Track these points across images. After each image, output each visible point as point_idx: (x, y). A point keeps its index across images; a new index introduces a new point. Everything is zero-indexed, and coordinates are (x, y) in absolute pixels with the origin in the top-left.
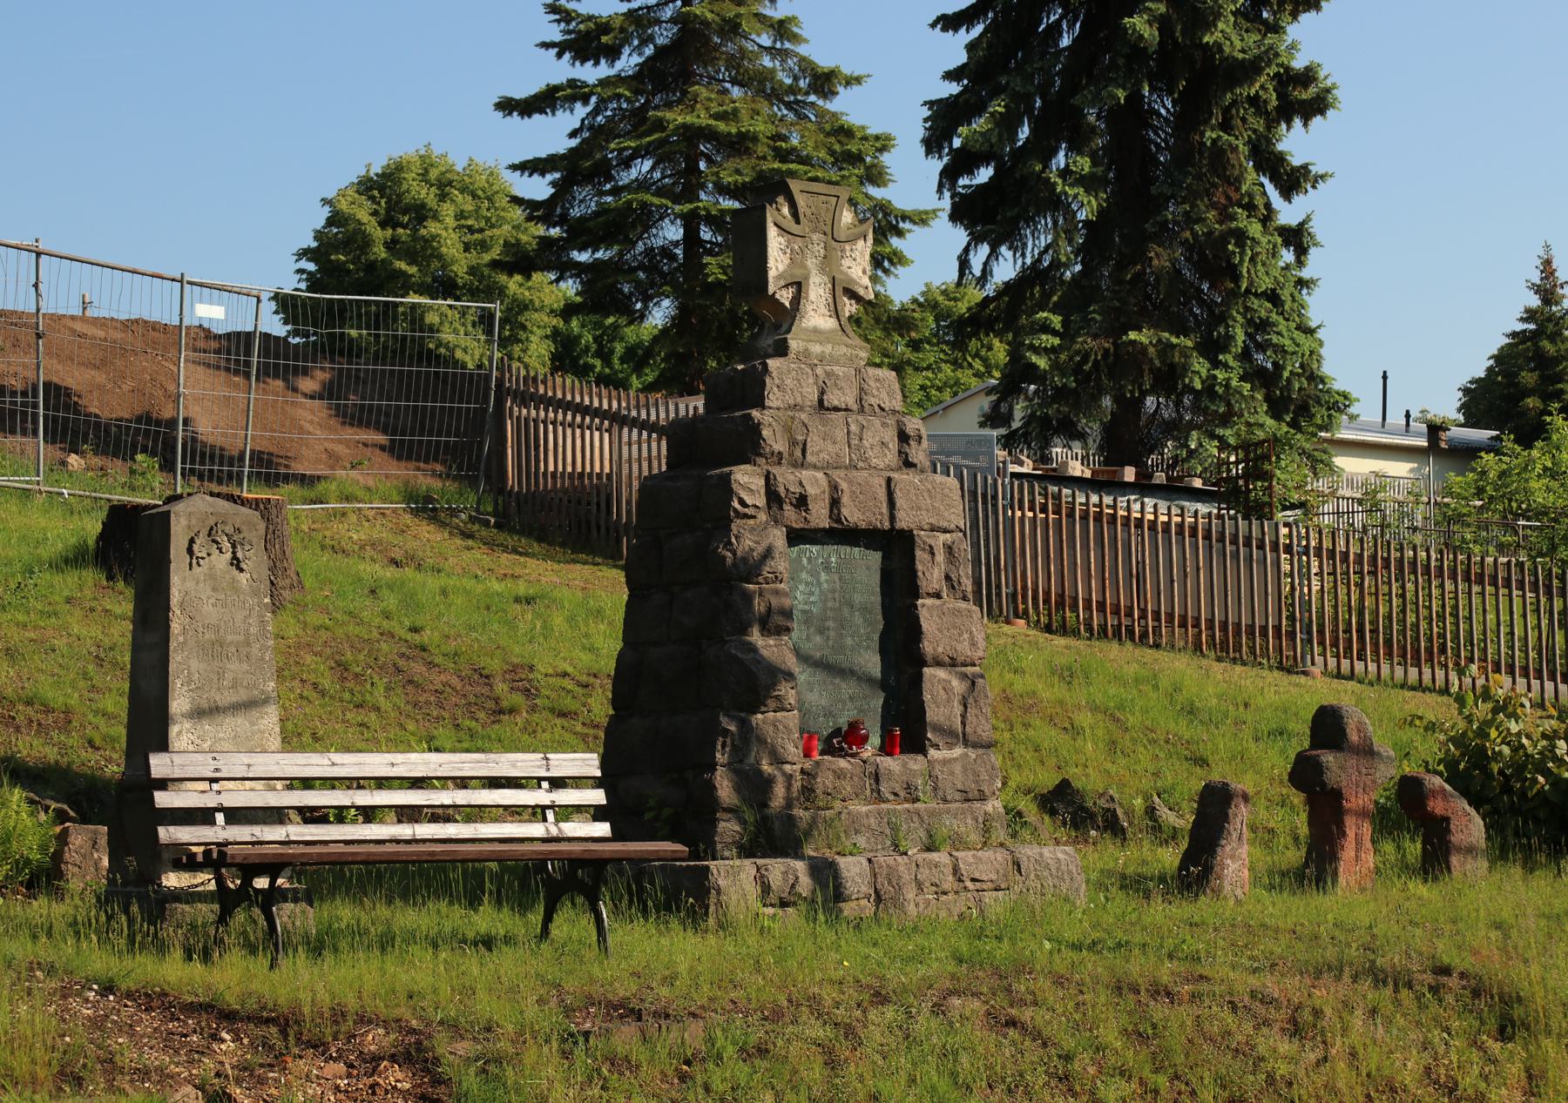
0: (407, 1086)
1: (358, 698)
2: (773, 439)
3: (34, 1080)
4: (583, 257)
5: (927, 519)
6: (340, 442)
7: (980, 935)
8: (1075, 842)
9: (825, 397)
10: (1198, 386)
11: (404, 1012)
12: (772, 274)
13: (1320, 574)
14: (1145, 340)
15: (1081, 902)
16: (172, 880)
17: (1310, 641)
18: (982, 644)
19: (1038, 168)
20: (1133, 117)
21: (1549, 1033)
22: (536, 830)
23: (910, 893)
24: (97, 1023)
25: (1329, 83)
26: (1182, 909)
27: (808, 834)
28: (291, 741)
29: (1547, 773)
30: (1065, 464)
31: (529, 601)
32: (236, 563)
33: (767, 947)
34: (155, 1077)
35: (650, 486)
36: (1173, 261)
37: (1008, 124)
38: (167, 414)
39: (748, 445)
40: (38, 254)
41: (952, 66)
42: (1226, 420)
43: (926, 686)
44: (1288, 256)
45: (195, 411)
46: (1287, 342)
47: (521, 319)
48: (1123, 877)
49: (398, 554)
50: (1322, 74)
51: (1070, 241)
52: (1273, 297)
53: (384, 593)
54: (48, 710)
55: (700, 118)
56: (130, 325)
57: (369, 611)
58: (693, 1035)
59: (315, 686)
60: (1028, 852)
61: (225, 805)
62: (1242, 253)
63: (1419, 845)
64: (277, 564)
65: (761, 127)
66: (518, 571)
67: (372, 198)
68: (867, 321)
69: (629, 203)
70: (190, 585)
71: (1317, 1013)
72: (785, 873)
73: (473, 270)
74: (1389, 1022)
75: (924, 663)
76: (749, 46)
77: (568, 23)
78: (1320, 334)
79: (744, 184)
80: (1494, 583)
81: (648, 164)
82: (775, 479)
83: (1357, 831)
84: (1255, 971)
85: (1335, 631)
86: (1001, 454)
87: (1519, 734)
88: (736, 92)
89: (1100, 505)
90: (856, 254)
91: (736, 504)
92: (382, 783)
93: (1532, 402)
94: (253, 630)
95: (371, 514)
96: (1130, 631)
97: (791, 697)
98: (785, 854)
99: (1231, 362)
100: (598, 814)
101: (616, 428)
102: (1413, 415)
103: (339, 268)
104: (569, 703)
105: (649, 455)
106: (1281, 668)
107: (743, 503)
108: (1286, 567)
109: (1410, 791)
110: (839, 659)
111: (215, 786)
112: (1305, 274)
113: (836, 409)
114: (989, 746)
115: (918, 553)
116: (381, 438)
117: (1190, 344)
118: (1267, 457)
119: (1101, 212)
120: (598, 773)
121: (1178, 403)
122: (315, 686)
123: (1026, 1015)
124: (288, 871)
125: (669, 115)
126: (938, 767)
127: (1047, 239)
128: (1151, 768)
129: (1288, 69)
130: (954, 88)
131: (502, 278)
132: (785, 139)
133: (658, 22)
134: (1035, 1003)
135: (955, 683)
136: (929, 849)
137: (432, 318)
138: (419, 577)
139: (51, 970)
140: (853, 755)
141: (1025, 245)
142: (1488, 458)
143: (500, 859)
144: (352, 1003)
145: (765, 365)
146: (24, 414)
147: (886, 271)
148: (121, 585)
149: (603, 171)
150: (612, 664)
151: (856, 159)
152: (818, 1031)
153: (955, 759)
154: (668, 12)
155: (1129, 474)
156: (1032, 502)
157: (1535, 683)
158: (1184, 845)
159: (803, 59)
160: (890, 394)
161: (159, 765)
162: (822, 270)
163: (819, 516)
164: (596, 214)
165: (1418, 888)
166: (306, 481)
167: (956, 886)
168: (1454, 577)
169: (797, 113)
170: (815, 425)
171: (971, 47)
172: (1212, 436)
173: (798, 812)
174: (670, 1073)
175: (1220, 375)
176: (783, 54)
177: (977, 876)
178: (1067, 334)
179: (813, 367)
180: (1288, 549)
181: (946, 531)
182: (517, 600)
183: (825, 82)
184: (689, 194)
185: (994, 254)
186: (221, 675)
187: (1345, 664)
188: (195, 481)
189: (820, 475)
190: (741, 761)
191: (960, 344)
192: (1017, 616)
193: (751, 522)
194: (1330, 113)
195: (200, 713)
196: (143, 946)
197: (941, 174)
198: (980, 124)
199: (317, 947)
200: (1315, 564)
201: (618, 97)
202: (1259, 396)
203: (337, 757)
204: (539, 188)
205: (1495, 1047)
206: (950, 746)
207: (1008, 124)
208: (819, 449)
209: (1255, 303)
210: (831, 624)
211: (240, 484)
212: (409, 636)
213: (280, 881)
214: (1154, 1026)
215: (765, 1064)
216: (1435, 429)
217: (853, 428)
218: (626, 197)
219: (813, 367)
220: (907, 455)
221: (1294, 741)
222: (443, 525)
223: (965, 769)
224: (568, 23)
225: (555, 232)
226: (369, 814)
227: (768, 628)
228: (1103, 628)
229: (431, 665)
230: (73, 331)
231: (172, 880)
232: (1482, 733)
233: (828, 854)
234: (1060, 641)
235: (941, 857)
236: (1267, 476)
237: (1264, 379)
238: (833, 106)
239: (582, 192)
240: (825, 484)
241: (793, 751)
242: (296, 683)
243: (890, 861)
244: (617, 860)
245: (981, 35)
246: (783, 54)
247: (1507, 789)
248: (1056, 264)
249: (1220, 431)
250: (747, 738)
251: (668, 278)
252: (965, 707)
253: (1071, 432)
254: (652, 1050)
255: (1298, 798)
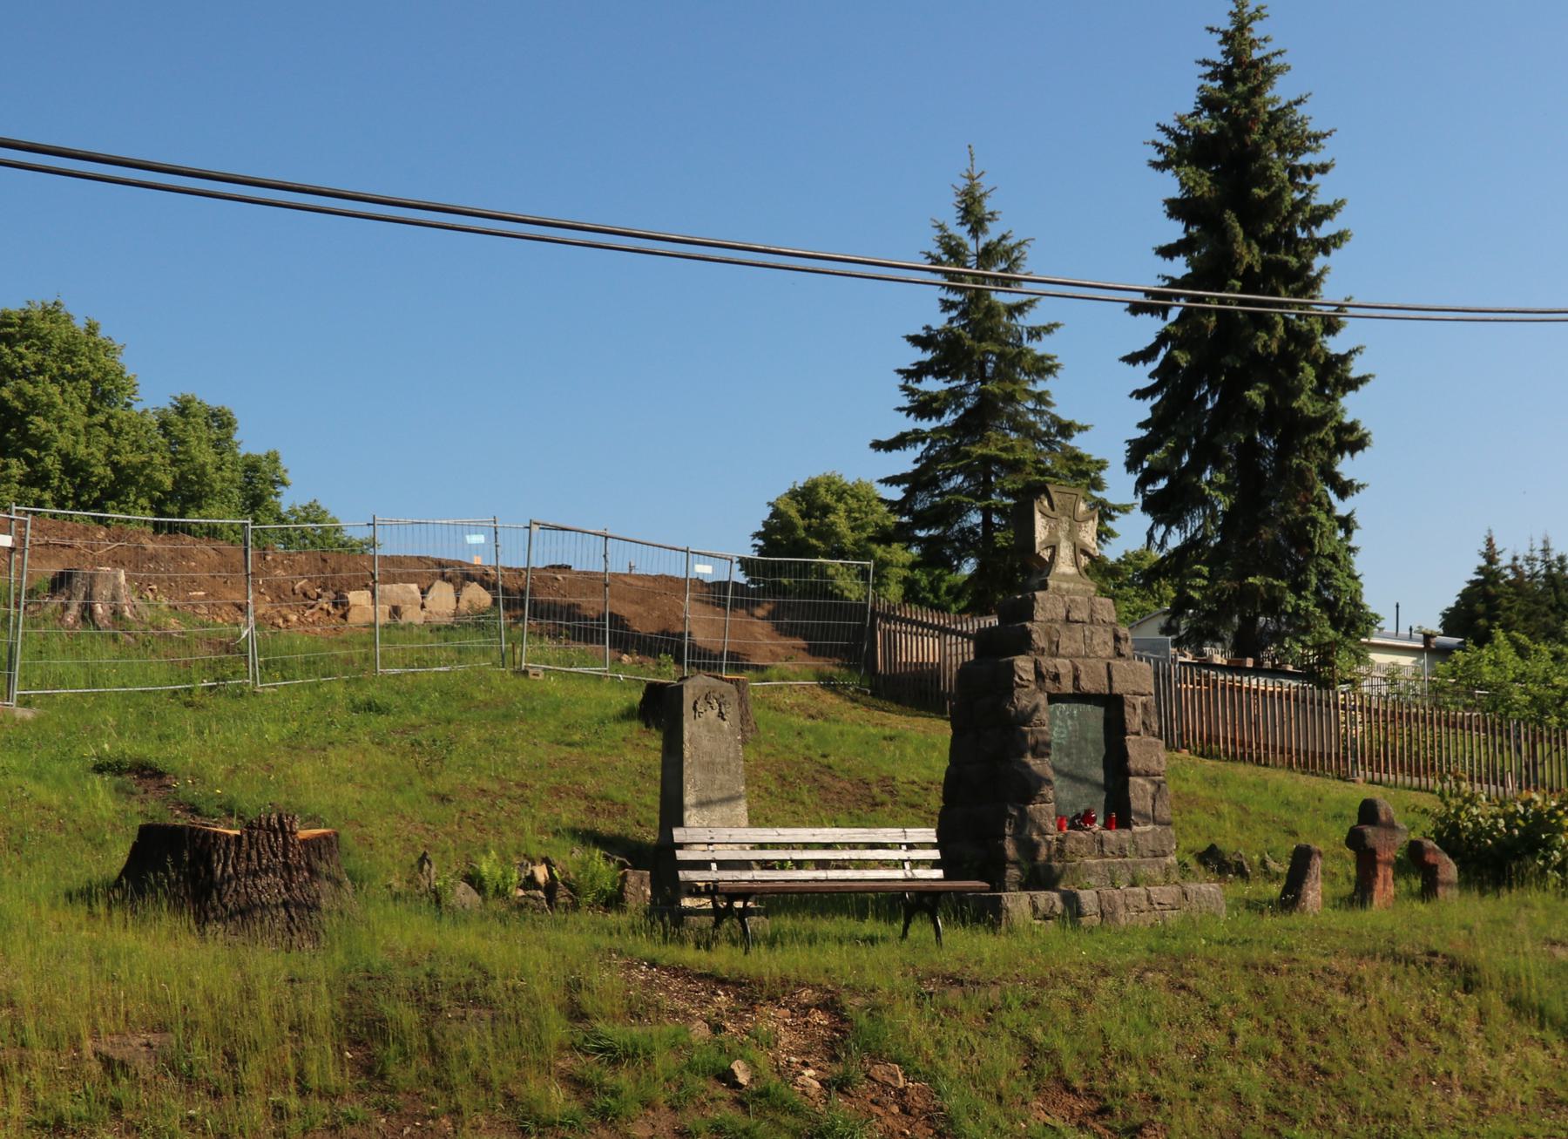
0: (826, 1023)
1: (791, 797)
2: (1039, 640)
3: (614, 1015)
4: (922, 534)
5: (1132, 688)
6: (779, 645)
7: (1163, 936)
8: (1218, 881)
10: (1290, 610)
11: (822, 980)
12: (1038, 541)
13: (1362, 722)
14: (1258, 582)
15: (1223, 916)
16: (687, 902)
17: (1356, 762)
18: (1164, 763)
19: (1195, 479)
20: (1250, 450)
21: (1491, 987)
22: (899, 874)
23: (1122, 911)
24: (647, 984)
25: (1365, 431)
26: (1282, 920)
28: (754, 822)
29: (1492, 838)
30: (1211, 656)
31: (891, 738)
32: (721, 715)
33: (1036, 943)
34: (681, 1016)
35: (965, 670)
36: (1275, 536)
37: (1176, 454)
38: (678, 629)
39: (1023, 644)
40: (606, 538)
41: (1142, 419)
42: (1306, 630)
43: (1131, 788)
44: (1341, 534)
45: (694, 628)
46: (1342, 585)
47: (885, 572)
48: (1248, 902)
49: (814, 712)
50: (1361, 427)
51: (1213, 522)
52: (1333, 558)
53: (806, 734)
54: (614, 804)
55: (992, 451)
56: (656, 578)
57: (798, 745)
58: (994, 994)
59: (766, 789)
60: (1192, 887)
61: (718, 858)
62: (1315, 532)
63: (1419, 881)
64: (744, 718)
65: (1027, 456)
66: (885, 721)
67: (798, 502)
68: (1093, 570)
69: (950, 501)
70: (695, 729)
71: (1361, 979)
72: (1047, 900)
73: (856, 543)
74: (1402, 984)
75: (1130, 775)
76: (1021, 409)
77: (913, 396)
78: (1361, 580)
79: (1018, 490)
80: (1462, 727)
81: (960, 479)
83: (1384, 873)
84: (1326, 955)
85: (1371, 756)
86: (1173, 650)
87: (1477, 816)
88: (1013, 435)
89: (1232, 681)
90: (1088, 529)
91: (1017, 679)
92: (807, 846)
93: (1482, 622)
94: (731, 755)
95: (797, 688)
96: (1251, 755)
97: (1050, 795)
98: (1046, 889)
99: (1309, 596)
100: (935, 864)
101: (942, 637)
102: (1414, 629)
103: (778, 542)
104: (916, 799)
105: (964, 651)
106: (1339, 778)
107: (1021, 678)
108: (1342, 719)
109: (1415, 849)
110: (1079, 772)
111: (711, 848)
112: (1352, 544)
113: (1077, 622)
114: (1169, 824)
115: (1126, 708)
116: (801, 643)
117: (1285, 585)
118: (1331, 653)
119: (1232, 506)
120: (935, 840)
121: (1278, 621)
122: (766, 789)
123: (1192, 982)
124: (753, 898)
125: (973, 449)
127: (1198, 523)
128: (1264, 837)
129: (1340, 423)
130: (1144, 433)
131: (874, 546)
132: (1043, 463)
133: (967, 395)
134: (1196, 976)
135: (1148, 786)
136: (1133, 885)
137: (831, 571)
138: (827, 725)
139: (620, 953)
140: (1088, 830)
141: (1186, 526)
142: (1458, 653)
143: (875, 891)
144: (793, 974)
145: (1034, 596)
146: (598, 631)
147: (1104, 541)
148: (654, 730)
149: (934, 483)
150: (943, 776)
151: (1085, 474)
152: (1067, 992)
154: (973, 389)
155: (1250, 663)
156: (1192, 680)
157: (1485, 786)
158: (1283, 882)
159: (1053, 416)
160: (1109, 613)
161: (678, 835)
162: (1068, 539)
163: (1067, 686)
164: (930, 508)
165: (1420, 907)
166: (758, 668)
168: (1439, 724)
169: (1050, 448)
170: (1065, 633)
171: (1154, 409)
172: (1298, 641)
173: (1055, 864)
174: (980, 1016)
175: (1302, 604)
176: (1042, 413)
178: (1212, 579)
179: (1063, 596)
180: (1344, 707)
182: (885, 738)
183: (1066, 429)
184: (986, 495)
185: (1168, 531)
186: (713, 782)
187: (1377, 775)
188: (694, 670)
189: (1067, 661)
190: (1020, 833)
191: (1147, 585)
192: (1183, 747)
194: (1366, 449)
195: (701, 804)
196: (671, 940)
197: (1137, 483)
198: (1159, 454)
199: (772, 942)
200: (1359, 717)
201: (943, 439)
202: (1325, 617)
203: (781, 831)
204: (896, 493)
205: (1461, 996)
206: (1145, 824)
207: (1176, 454)
208: (1066, 645)
209: (1323, 561)
210: (1074, 751)
211: (721, 671)
212: (821, 760)
213: (749, 904)
214: (1266, 988)
215: (1037, 1011)
216: (1428, 637)
218: (947, 497)
219: (1063, 596)
221: (1348, 822)
222: (839, 694)
223: (1154, 839)
224: (913, 396)
225: (905, 519)
226: (799, 864)
227: (1036, 755)
228: (1234, 754)
229: (834, 777)
230: (625, 583)
231: (687, 902)
232: (1457, 815)
233: (1073, 888)
234: (1209, 762)
235: (1139, 890)
236: (1331, 664)
237: (1328, 606)
238: (1071, 443)
239: (921, 495)
240: (1070, 667)
241: (1051, 827)
242: (756, 788)
243: (1110, 892)
244: (947, 892)
245: (1160, 402)
246: (1042, 413)
247: (1470, 848)
248: (1205, 537)
249: (1302, 638)
250: (1024, 820)
251: (973, 546)
253: (1216, 638)
254: (970, 1003)
255: (1349, 854)
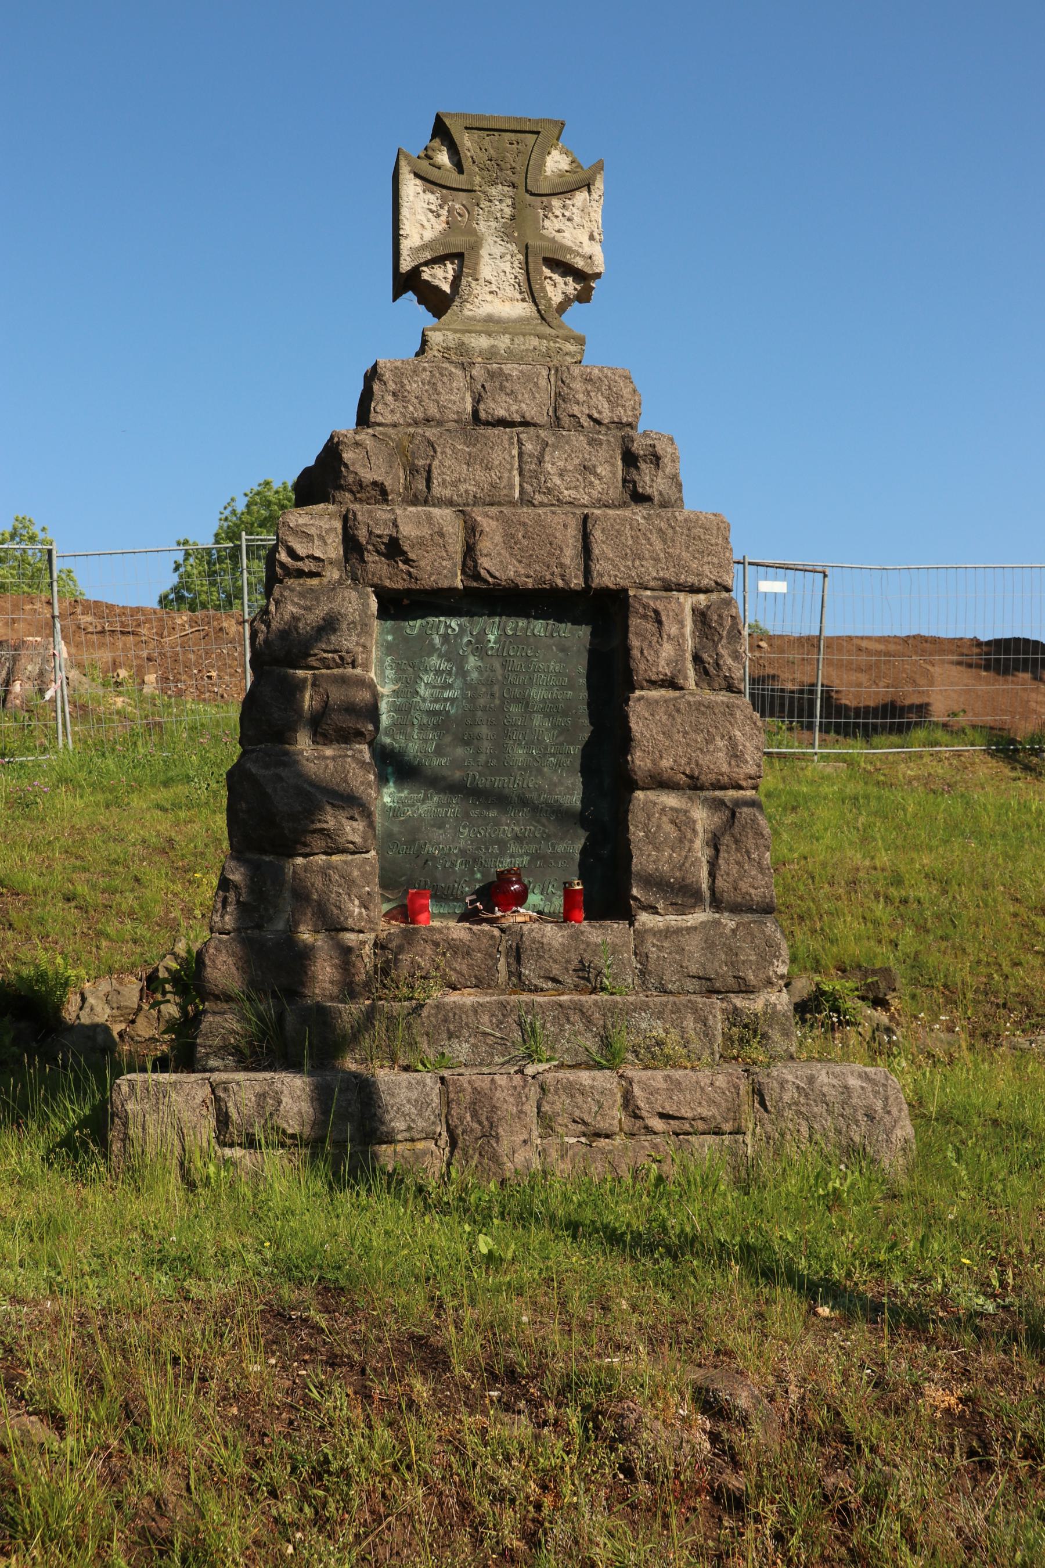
5: (651, 572)
9: (482, 406)
27: (355, 1038)
82: (355, 519)
97: (353, 830)
107: (292, 553)
115: (634, 622)
126: (650, 940)
153: (690, 930)
167: (628, 1123)
177: (670, 1109)
181: (694, 590)
190: (259, 927)
193: (315, 581)
210: (484, 730)
217: (529, 447)
220: (634, 483)
227: (321, 734)
252: (717, 850)
